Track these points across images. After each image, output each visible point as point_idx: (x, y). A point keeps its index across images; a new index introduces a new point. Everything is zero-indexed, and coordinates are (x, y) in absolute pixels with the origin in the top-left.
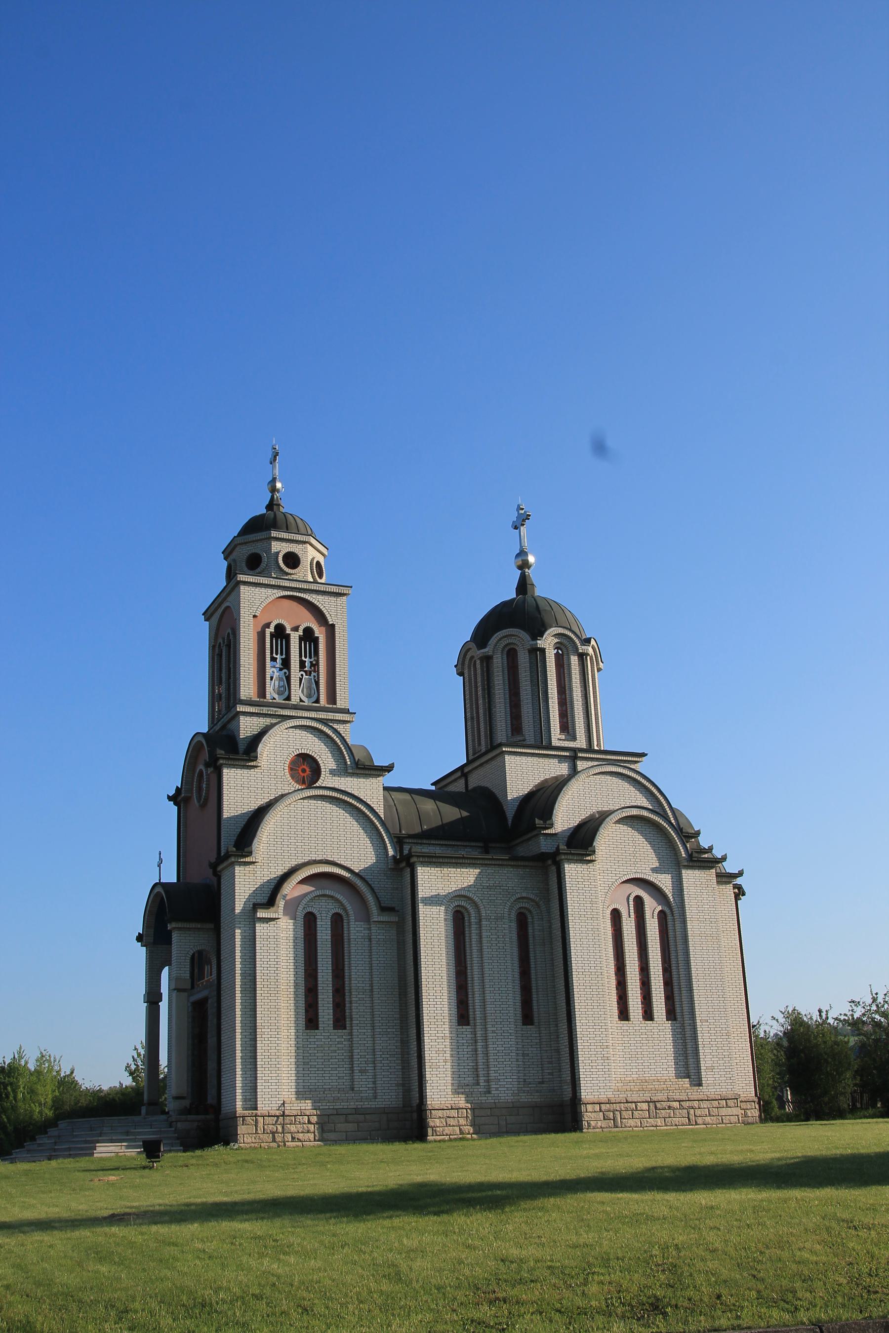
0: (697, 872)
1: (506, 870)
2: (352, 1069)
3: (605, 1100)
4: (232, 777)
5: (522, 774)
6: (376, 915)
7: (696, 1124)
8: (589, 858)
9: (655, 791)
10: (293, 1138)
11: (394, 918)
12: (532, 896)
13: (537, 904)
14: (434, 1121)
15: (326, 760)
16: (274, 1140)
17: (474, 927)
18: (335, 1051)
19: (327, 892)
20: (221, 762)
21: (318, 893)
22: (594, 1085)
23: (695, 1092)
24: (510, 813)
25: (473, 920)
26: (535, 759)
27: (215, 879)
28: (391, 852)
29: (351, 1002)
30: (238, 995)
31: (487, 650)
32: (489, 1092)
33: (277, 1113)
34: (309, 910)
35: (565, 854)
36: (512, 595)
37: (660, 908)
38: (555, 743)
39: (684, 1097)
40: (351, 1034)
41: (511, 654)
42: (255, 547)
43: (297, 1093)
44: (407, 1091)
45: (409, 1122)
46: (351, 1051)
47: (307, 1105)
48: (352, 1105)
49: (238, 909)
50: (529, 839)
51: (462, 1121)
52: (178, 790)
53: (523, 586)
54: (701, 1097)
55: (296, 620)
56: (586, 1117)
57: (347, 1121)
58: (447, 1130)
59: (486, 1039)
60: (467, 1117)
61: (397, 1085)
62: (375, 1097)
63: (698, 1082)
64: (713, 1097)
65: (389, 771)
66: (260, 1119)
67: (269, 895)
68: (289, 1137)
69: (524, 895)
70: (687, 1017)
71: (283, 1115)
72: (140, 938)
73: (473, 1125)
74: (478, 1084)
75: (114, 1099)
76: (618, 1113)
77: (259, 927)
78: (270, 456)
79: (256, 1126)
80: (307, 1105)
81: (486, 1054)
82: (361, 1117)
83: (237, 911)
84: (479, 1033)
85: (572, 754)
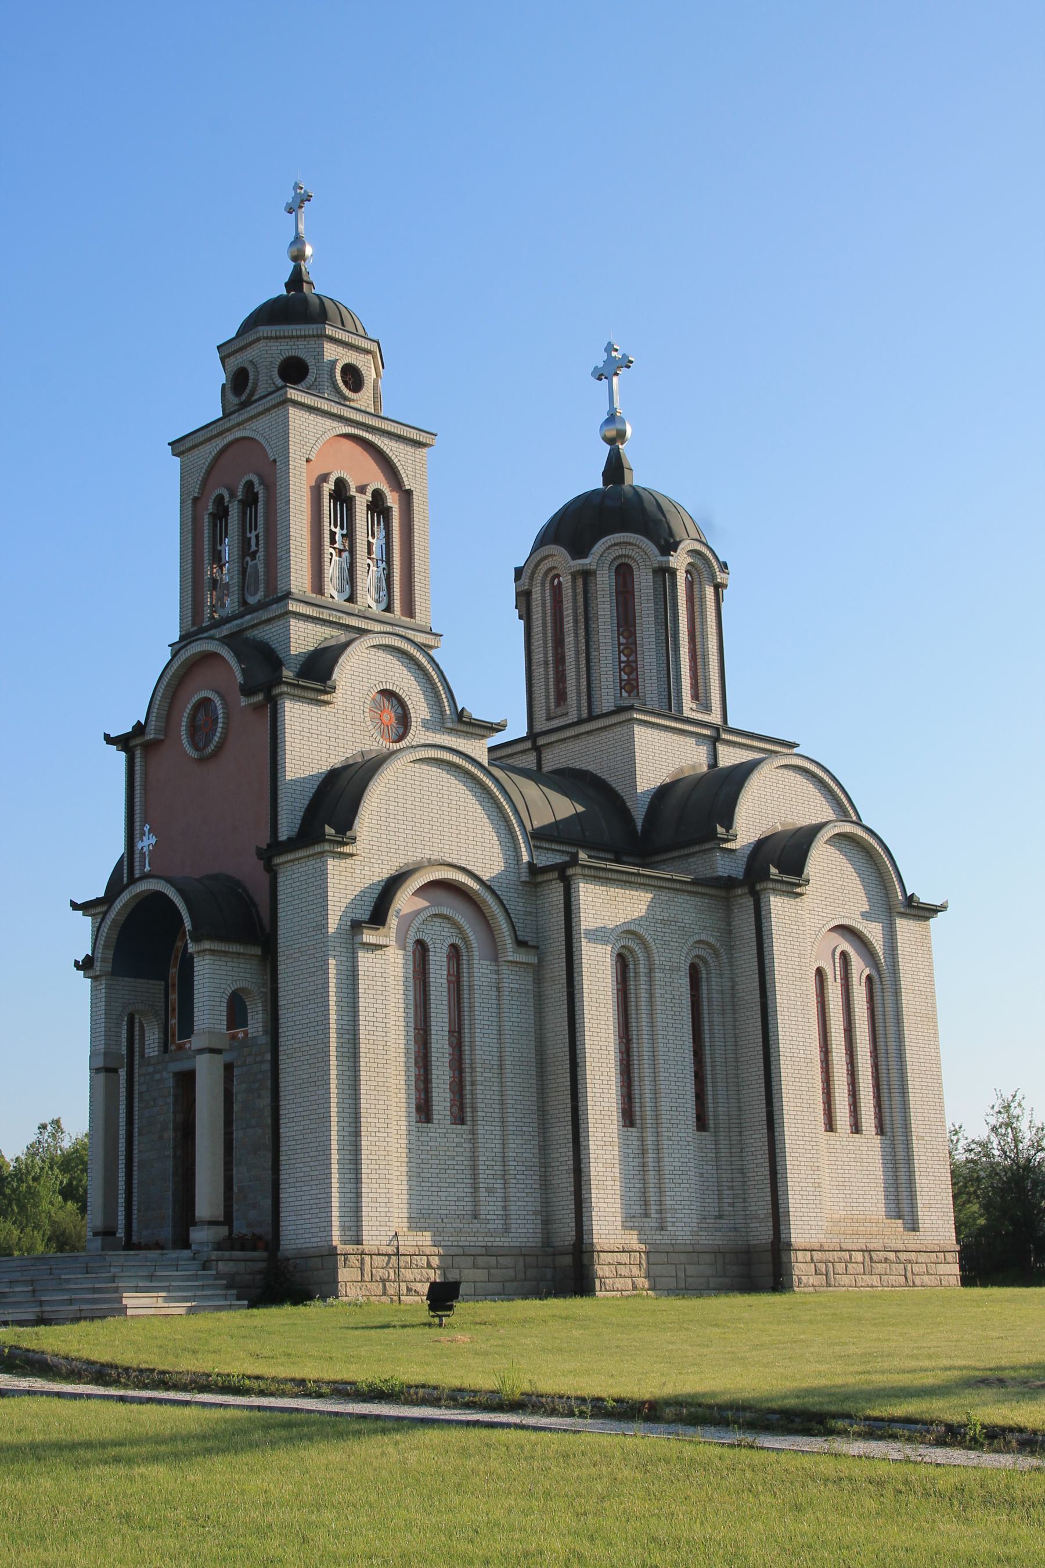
0: (911, 923)
1: (682, 898)
2: (475, 1188)
3: (816, 1246)
4: (297, 716)
5: (659, 758)
6: (511, 953)
7: (914, 1285)
8: (798, 890)
9: (844, 800)
10: (409, 1290)
12: (712, 940)
16: (385, 1294)
17: (643, 979)
18: (453, 1158)
19: (446, 911)
21: (434, 911)
22: (805, 1226)
23: (912, 1240)
24: (639, 814)
25: (642, 969)
27: (265, 878)
28: (526, 858)
30: (333, 1063)
32: (662, 1228)
33: (390, 1250)
34: (420, 936)
35: (583, 866)
36: (598, 483)
37: (867, 972)
39: (902, 1247)
40: (473, 1132)
41: (624, 573)
42: (288, 341)
45: (565, 1270)
46: (474, 1159)
47: (425, 1239)
48: (481, 1241)
50: (693, 854)
51: (635, 1271)
53: (615, 469)
57: (475, 1266)
58: (619, 1283)
59: (658, 1150)
60: (640, 1264)
61: (535, 1213)
62: (507, 1230)
63: (913, 1227)
64: (931, 1248)
65: (498, 730)
66: (367, 1258)
67: (378, 908)
68: (403, 1286)
71: (397, 1254)
72: (85, 965)
73: (648, 1276)
74: (647, 1215)
76: (830, 1265)
78: (289, 197)
79: (362, 1270)
80: (425, 1239)
81: (659, 1171)
82: (492, 1261)
83: (331, 930)
84: (650, 1140)
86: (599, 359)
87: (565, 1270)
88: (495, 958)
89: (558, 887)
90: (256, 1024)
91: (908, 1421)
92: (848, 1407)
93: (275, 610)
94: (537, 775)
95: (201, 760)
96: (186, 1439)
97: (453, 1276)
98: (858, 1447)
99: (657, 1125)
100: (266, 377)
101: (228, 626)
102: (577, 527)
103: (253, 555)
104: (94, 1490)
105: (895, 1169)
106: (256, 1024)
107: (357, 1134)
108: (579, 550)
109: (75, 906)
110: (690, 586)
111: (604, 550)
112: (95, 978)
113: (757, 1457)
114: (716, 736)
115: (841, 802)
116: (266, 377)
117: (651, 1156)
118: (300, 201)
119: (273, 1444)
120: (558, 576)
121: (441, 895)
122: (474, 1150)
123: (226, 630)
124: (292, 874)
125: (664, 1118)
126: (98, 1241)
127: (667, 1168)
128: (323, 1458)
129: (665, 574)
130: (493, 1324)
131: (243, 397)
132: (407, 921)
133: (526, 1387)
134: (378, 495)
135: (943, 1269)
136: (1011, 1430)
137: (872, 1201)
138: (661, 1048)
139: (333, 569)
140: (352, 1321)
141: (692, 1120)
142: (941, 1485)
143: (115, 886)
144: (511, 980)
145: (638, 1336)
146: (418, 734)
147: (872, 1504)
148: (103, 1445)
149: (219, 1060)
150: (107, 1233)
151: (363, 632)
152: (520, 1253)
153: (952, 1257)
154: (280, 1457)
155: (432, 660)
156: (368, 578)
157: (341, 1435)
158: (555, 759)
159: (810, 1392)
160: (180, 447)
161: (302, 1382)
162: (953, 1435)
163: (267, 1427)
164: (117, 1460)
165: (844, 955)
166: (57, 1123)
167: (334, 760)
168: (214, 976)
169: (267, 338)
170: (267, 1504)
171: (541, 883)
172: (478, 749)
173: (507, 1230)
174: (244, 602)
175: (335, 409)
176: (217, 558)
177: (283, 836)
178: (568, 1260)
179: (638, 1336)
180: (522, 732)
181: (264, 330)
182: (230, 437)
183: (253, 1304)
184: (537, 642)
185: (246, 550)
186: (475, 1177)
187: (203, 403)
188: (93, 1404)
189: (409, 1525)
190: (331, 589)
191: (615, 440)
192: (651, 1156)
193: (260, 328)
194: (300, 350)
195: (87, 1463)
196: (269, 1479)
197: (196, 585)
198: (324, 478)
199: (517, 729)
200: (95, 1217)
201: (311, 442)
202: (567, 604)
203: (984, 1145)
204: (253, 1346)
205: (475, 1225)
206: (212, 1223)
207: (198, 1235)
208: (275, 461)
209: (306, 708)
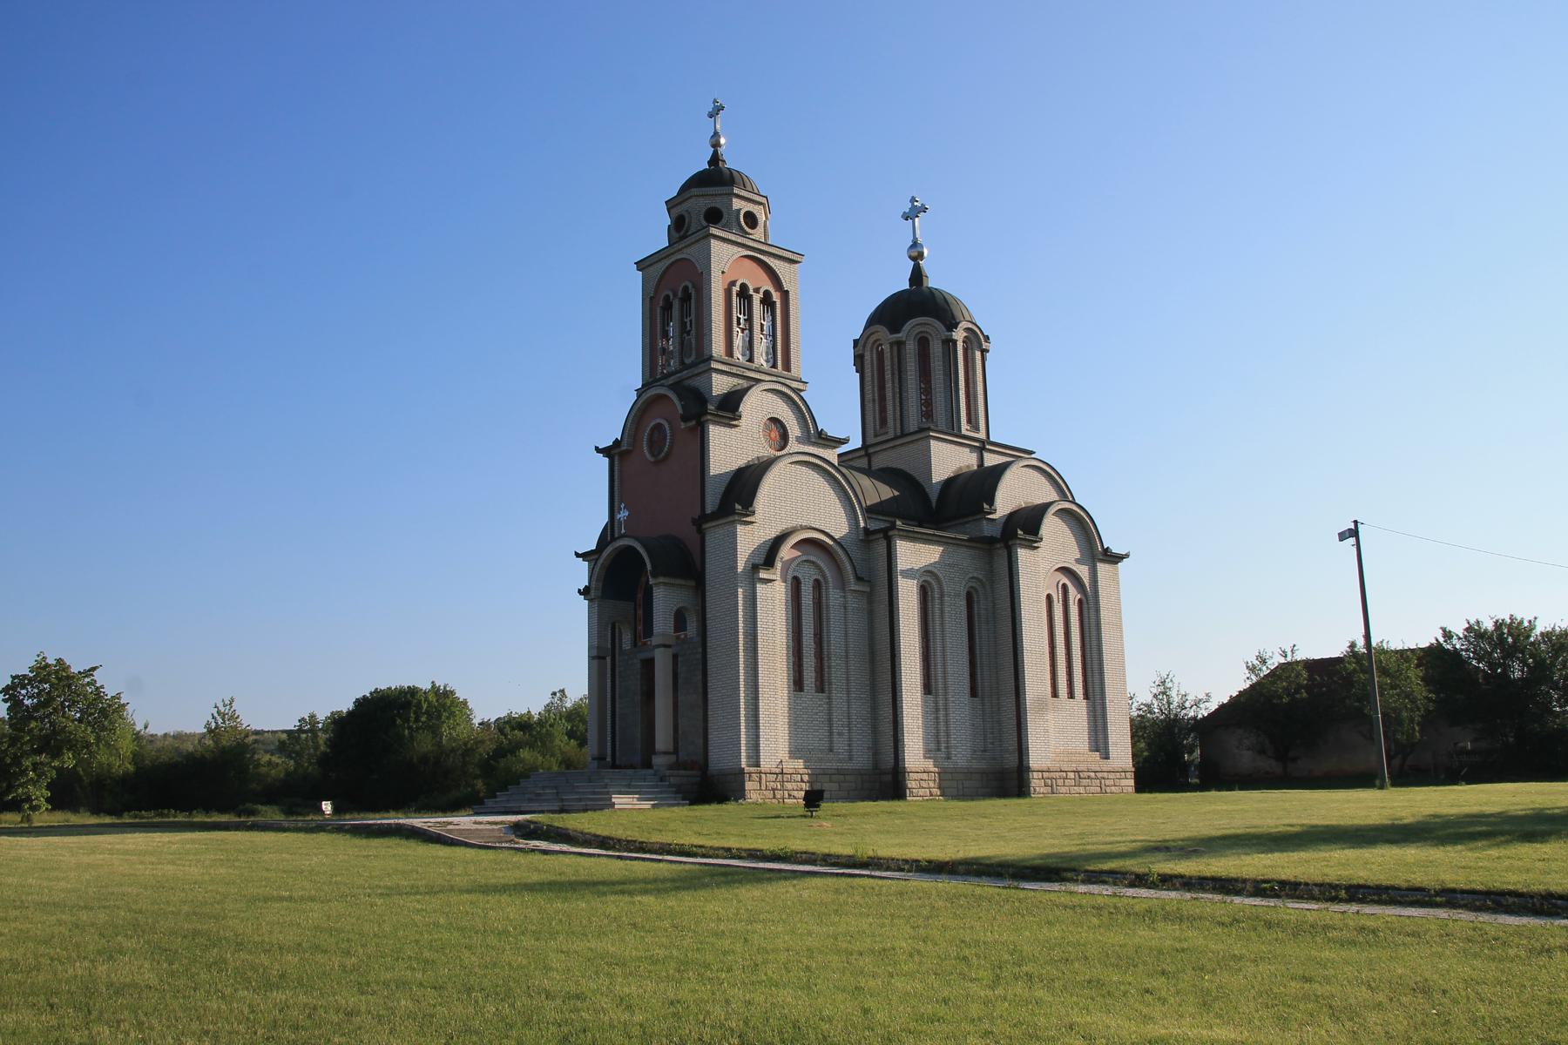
2: (831, 733)
4: (716, 433)
5: (947, 460)
6: (853, 585)
15: (794, 430)
19: (812, 558)
23: (1106, 765)
24: (934, 496)
30: (741, 654)
31: (901, 335)
36: (906, 286)
38: (964, 432)
41: (923, 343)
44: (876, 751)
45: (887, 782)
46: (830, 714)
47: (800, 764)
48: (835, 765)
49: (740, 567)
53: (917, 276)
55: (757, 281)
56: (911, 784)
58: (921, 792)
59: (946, 709)
62: (851, 759)
72: (585, 592)
75: (203, 756)
77: (760, 587)
80: (800, 764)
81: (947, 722)
84: (941, 703)
86: (907, 207)
87: (887, 782)
89: (884, 543)
90: (692, 629)
91: (1111, 872)
92: (1074, 864)
93: (702, 367)
94: (868, 472)
95: (657, 463)
96: (664, 880)
97: (817, 787)
98: (1082, 888)
99: (946, 693)
100: (696, 220)
102: (892, 314)
103: (688, 333)
104: (612, 910)
106: (692, 629)
107: (756, 698)
108: (895, 329)
109: (578, 555)
110: (965, 351)
111: (912, 327)
112: (590, 601)
113: (1022, 894)
114: (982, 447)
115: (1063, 490)
116: (696, 220)
117: (942, 713)
118: (716, 111)
119: (718, 885)
121: (809, 548)
122: (830, 709)
123: (671, 380)
124: (714, 536)
125: (951, 689)
126: (595, 763)
128: (750, 894)
129: (950, 343)
130: (845, 816)
132: (787, 565)
133: (871, 853)
134: (767, 293)
135: (1124, 782)
136: (1176, 877)
137: (1081, 741)
138: (948, 645)
139: (739, 340)
140: (756, 814)
141: (967, 690)
142: (1137, 908)
143: (603, 541)
144: (853, 602)
145: (931, 824)
146: (793, 446)
147: (1095, 921)
148: (613, 883)
149: (670, 652)
150: (600, 758)
151: (758, 381)
153: (1131, 775)
154: (723, 893)
155: (802, 399)
156: (761, 346)
157: (759, 880)
158: (879, 462)
159: (1049, 856)
160: (642, 265)
161: (729, 850)
162: (1140, 880)
163: (712, 875)
164: (623, 892)
165: (1064, 586)
166: (562, 691)
167: (741, 462)
168: (665, 600)
170: (719, 919)
172: (832, 455)
173: (851, 759)
174: (682, 362)
175: (740, 240)
176: (665, 335)
177: (708, 511)
178: (889, 778)
179: (931, 824)
180: (858, 444)
181: (695, 191)
182: (673, 259)
183: (692, 803)
184: (868, 388)
185: (684, 330)
186: (831, 725)
187: (655, 236)
188: (604, 860)
189: (810, 934)
190: (738, 354)
191: (917, 257)
192: (942, 713)
194: (717, 203)
195: (604, 894)
196: (717, 905)
197: (652, 352)
198: (733, 283)
199: (856, 442)
200: (591, 749)
201: (724, 260)
202: (887, 363)
203: (1148, 706)
204: (696, 827)
205: (831, 756)
206: (666, 753)
207: (657, 760)
209: (723, 429)
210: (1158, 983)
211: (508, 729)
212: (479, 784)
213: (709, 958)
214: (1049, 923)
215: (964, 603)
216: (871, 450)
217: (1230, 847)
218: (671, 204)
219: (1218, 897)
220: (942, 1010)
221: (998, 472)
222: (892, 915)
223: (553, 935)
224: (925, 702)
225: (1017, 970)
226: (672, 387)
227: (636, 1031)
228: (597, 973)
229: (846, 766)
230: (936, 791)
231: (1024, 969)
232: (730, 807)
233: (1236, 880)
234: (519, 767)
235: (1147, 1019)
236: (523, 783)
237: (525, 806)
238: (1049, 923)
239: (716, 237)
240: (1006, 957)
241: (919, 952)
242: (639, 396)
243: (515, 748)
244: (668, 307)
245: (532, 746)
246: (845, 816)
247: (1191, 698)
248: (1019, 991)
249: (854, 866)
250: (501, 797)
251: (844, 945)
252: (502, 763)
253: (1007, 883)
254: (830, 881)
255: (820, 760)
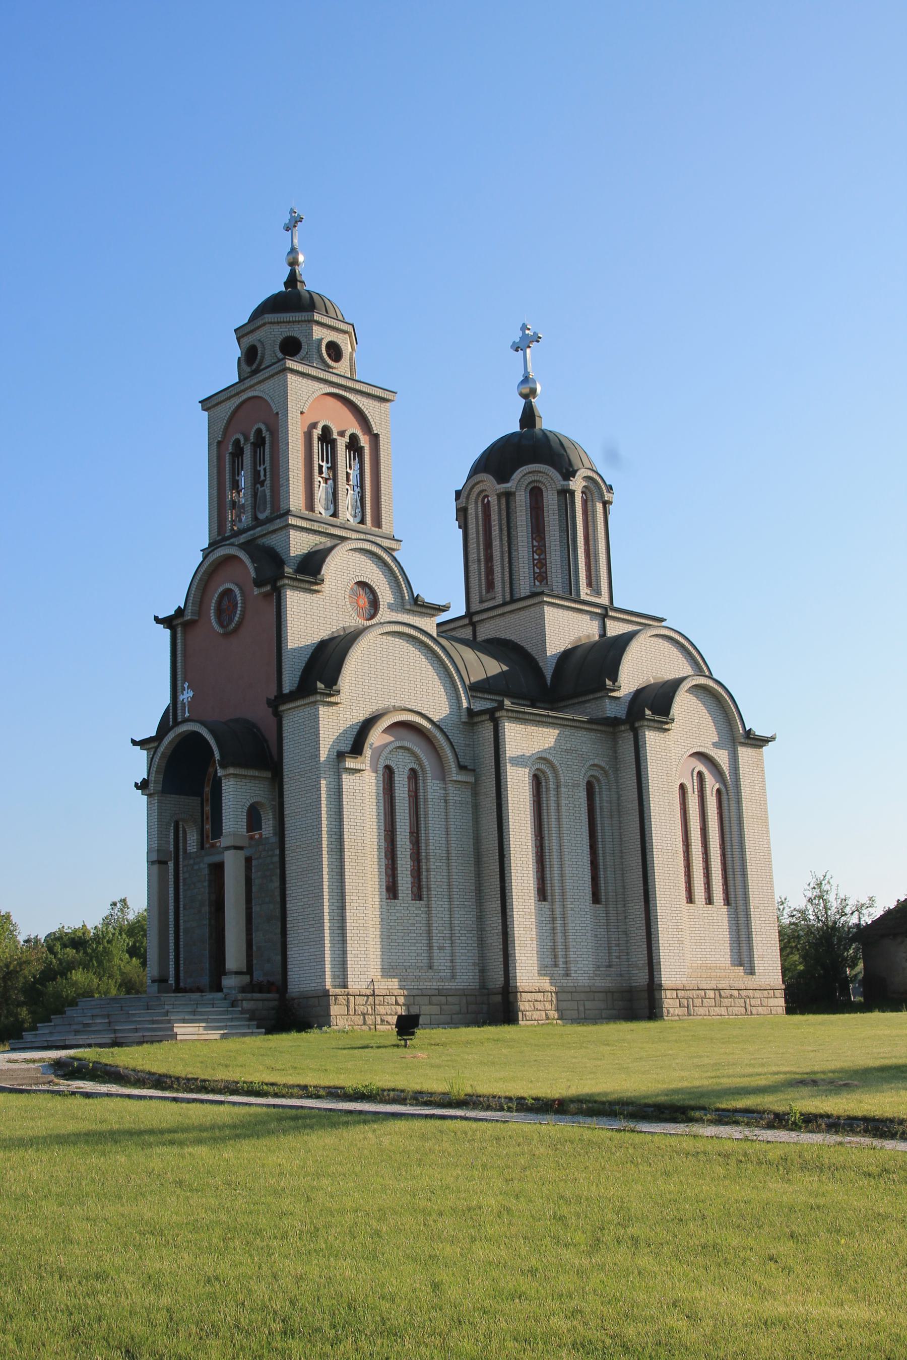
1: (581, 733)
2: (430, 947)
4: (295, 601)
5: (563, 630)
6: (455, 774)
7: (752, 1014)
10: (382, 1021)
11: (471, 779)
12: (603, 764)
13: (606, 772)
14: (524, 1004)
15: (386, 595)
16: (365, 1024)
19: (407, 744)
20: (286, 581)
21: (398, 744)
23: (750, 982)
24: (548, 672)
25: (552, 786)
26: (570, 613)
27: (272, 720)
29: (428, 870)
32: (567, 975)
33: (368, 992)
34: (388, 762)
36: (517, 428)
37: (717, 786)
38: (583, 596)
39: (743, 987)
40: (428, 906)
41: (536, 494)
43: (383, 970)
45: (497, 1005)
46: (429, 925)
47: (394, 984)
49: (324, 755)
52: (180, 612)
53: (529, 417)
54: (755, 987)
55: (343, 423)
56: (524, 1005)
57: (430, 1004)
58: (536, 1015)
59: (564, 918)
60: (552, 1001)
61: (474, 964)
62: (453, 977)
65: (444, 611)
66: (352, 998)
68: (378, 1018)
69: (596, 762)
70: (741, 902)
71: (373, 995)
72: (143, 786)
73: (557, 1010)
74: (556, 965)
77: (346, 779)
78: (286, 219)
79: (348, 1006)
80: (394, 984)
81: (565, 933)
82: (443, 999)
83: (322, 759)
85: (603, 612)
86: (517, 336)
87: (497, 1005)
88: (443, 779)
89: (490, 726)
90: (268, 828)
91: (747, 1111)
92: (703, 1102)
93: (278, 524)
94: (473, 644)
95: (226, 635)
96: (222, 1127)
97: (414, 1010)
99: (563, 900)
100: (271, 351)
101: (244, 535)
102: (500, 460)
103: (262, 483)
104: (156, 1164)
105: (738, 931)
106: (268, 828)
107: (343, 908)
108: (503, 477)
109: (134, 743)
110: (585, 502)
112: (149, 796)
113: (637, 1138)
114: (604, 614)
116: (271, 351)
117: (559, 923)
118: (294, 222)
119: (285, 1132)
120: (487, 496)
121: (403, 732)
122: (429, 919)
123: (242, 539)
124: (293, 718)
125: (569, 895)
126: (155, 987)
127: (571, 931)
128: (321, 1141)
129: (566, 494)
130: (444, 1045)
131: (254, 367)
132: (378, 752)
133: (469, 1090)
134: (353, 437)
135: (772, 1002)
136: (822, 1116)
139: (321, 492)
140: (341, 1044)
142: (770, 1156)
143: (164, 727)
144: (454, 794)
146: (385, 614)
147: (721, 1171)
148: (162, 1132)
149: (241, 855)
150: (161, 981)
151: (343, 539)
152: (463, 993)
153: (780, 994)
154: (290, 1141)
157: (334, 1125)
158: (486, 631)
160: (208, 404)
161: (305, 1087)
162: (779, 1121)
163: (280, 1119)
164: (172, 1143)
165: (700, 774)
166: (124, 901)
168: (236, 794)
169: (271, 323)
170: (281, 1174)
171: (476, 723)
172: (430, 624)
173: (453, 977)
174: (255, 518)
175: (322, 375)
176: (235, 485)
177: (286, 690)
178: (498, 998)
180: (462, 611)
181: (269, 317)
182: (244, 396)
183: (269, 1031)
185: (257, 480)
187: (225, 371)
189: (384, 1188)
190: (320, 507)
191: (528, 395)
192: (559, 923)
193: (266, 316)
194: (295, 331)
195: (150, 1145)
198: (314, 426)
199: (458, 609)
200: (153, 969)
201: (304, 400)
202: (494, 517)
203: (803, 912)
204: (269, 1061)
205: (430, 974)
206: (237, 973)
207: (228, 982)
208: (277, 413)
210: (785, 1248)
211: (58, 947)
212: (24, 1012)
213: (263, 1222)
214: (667, 1174)
215: (584, 794)
216: (476, 618)
217: (888, 1080)
218: (241, 333)
219: (867, 1141)
220: (526, 1284)
221: (623, 642)
222: (484, 1166)
223: (80, 1199)
224: (539, 912)
225: (621, 1231)
226: (243, 546)
227: (161, 1318)
228: (125, 1245)
229: (447, 985)
230: (554, 1014)
231: (630, 1231)
232: (312, 1036)
233: (892, 1121)
234: (70, 992)
235: (766, 1293)
236: (70, 1012)
237: (71, 1039)
238: (667, 1174)
239: (293, 371)
240: (610, 1216)
241: (508, 1210)
242: (205, 558)
243: (67, 968)
244: (238, 453)
245: (86, 967)
246: (444, 1045)
247: (851, 904)
248: (620, 1257)
249: (450, 1105)
250: (44, 1028)
251: (423, 1203)
252: (51, 987)
253: (623, 1124)
254: (417, 1124)
255: (418, 979)
